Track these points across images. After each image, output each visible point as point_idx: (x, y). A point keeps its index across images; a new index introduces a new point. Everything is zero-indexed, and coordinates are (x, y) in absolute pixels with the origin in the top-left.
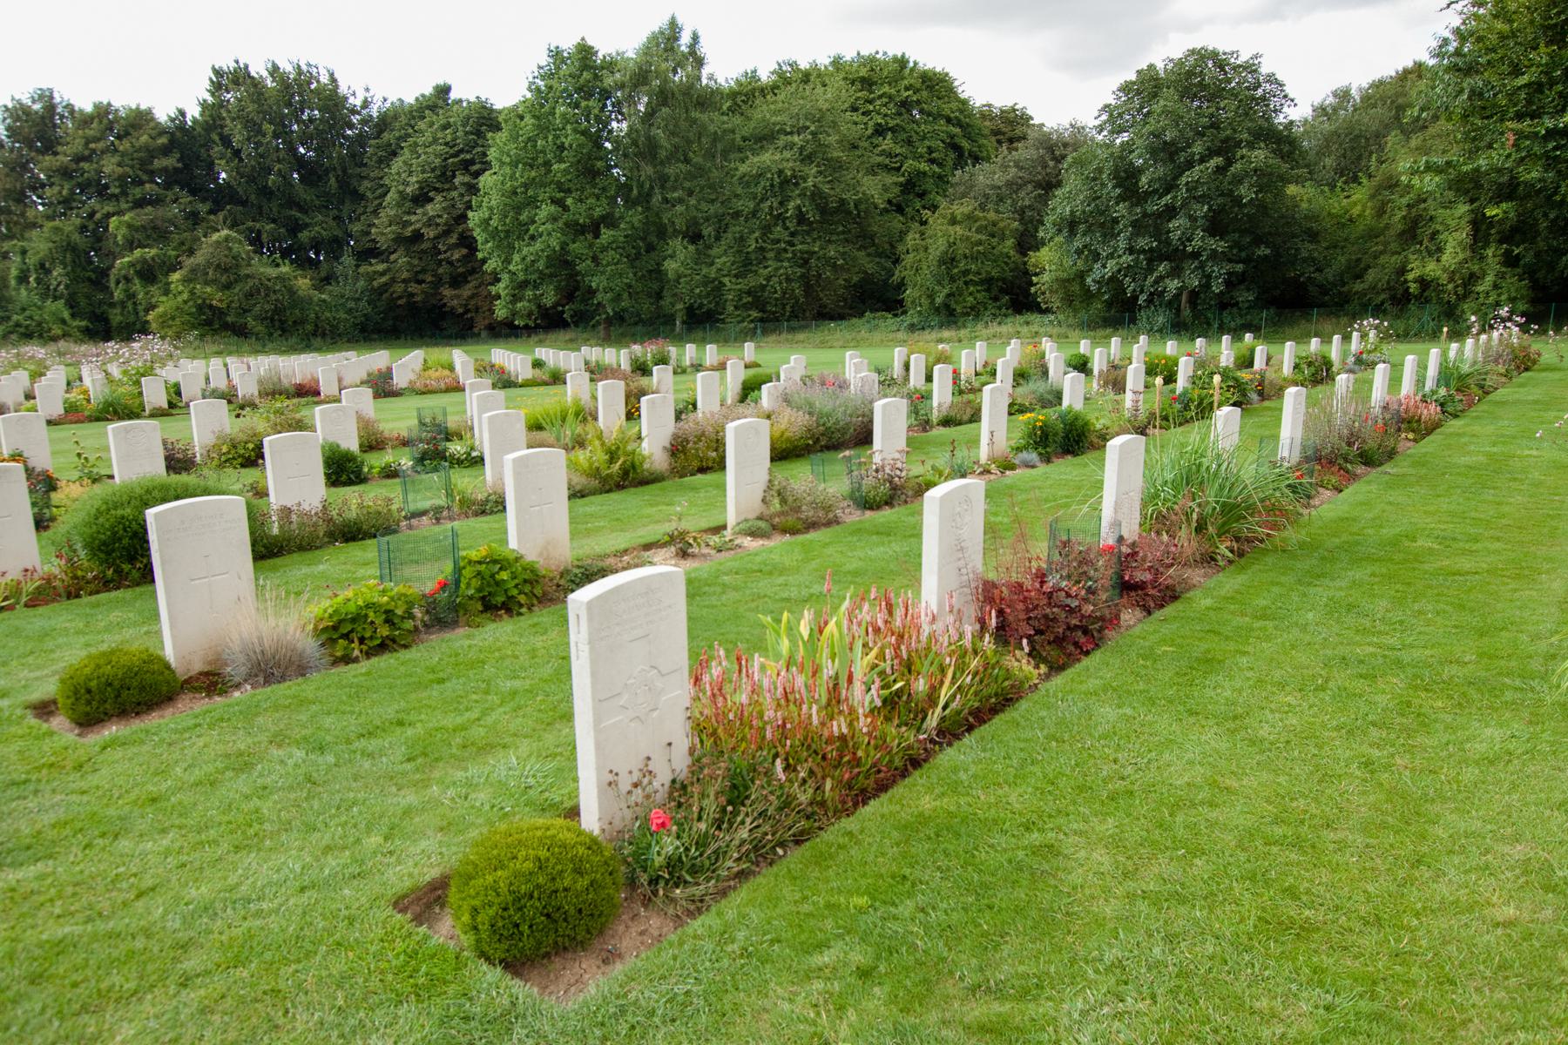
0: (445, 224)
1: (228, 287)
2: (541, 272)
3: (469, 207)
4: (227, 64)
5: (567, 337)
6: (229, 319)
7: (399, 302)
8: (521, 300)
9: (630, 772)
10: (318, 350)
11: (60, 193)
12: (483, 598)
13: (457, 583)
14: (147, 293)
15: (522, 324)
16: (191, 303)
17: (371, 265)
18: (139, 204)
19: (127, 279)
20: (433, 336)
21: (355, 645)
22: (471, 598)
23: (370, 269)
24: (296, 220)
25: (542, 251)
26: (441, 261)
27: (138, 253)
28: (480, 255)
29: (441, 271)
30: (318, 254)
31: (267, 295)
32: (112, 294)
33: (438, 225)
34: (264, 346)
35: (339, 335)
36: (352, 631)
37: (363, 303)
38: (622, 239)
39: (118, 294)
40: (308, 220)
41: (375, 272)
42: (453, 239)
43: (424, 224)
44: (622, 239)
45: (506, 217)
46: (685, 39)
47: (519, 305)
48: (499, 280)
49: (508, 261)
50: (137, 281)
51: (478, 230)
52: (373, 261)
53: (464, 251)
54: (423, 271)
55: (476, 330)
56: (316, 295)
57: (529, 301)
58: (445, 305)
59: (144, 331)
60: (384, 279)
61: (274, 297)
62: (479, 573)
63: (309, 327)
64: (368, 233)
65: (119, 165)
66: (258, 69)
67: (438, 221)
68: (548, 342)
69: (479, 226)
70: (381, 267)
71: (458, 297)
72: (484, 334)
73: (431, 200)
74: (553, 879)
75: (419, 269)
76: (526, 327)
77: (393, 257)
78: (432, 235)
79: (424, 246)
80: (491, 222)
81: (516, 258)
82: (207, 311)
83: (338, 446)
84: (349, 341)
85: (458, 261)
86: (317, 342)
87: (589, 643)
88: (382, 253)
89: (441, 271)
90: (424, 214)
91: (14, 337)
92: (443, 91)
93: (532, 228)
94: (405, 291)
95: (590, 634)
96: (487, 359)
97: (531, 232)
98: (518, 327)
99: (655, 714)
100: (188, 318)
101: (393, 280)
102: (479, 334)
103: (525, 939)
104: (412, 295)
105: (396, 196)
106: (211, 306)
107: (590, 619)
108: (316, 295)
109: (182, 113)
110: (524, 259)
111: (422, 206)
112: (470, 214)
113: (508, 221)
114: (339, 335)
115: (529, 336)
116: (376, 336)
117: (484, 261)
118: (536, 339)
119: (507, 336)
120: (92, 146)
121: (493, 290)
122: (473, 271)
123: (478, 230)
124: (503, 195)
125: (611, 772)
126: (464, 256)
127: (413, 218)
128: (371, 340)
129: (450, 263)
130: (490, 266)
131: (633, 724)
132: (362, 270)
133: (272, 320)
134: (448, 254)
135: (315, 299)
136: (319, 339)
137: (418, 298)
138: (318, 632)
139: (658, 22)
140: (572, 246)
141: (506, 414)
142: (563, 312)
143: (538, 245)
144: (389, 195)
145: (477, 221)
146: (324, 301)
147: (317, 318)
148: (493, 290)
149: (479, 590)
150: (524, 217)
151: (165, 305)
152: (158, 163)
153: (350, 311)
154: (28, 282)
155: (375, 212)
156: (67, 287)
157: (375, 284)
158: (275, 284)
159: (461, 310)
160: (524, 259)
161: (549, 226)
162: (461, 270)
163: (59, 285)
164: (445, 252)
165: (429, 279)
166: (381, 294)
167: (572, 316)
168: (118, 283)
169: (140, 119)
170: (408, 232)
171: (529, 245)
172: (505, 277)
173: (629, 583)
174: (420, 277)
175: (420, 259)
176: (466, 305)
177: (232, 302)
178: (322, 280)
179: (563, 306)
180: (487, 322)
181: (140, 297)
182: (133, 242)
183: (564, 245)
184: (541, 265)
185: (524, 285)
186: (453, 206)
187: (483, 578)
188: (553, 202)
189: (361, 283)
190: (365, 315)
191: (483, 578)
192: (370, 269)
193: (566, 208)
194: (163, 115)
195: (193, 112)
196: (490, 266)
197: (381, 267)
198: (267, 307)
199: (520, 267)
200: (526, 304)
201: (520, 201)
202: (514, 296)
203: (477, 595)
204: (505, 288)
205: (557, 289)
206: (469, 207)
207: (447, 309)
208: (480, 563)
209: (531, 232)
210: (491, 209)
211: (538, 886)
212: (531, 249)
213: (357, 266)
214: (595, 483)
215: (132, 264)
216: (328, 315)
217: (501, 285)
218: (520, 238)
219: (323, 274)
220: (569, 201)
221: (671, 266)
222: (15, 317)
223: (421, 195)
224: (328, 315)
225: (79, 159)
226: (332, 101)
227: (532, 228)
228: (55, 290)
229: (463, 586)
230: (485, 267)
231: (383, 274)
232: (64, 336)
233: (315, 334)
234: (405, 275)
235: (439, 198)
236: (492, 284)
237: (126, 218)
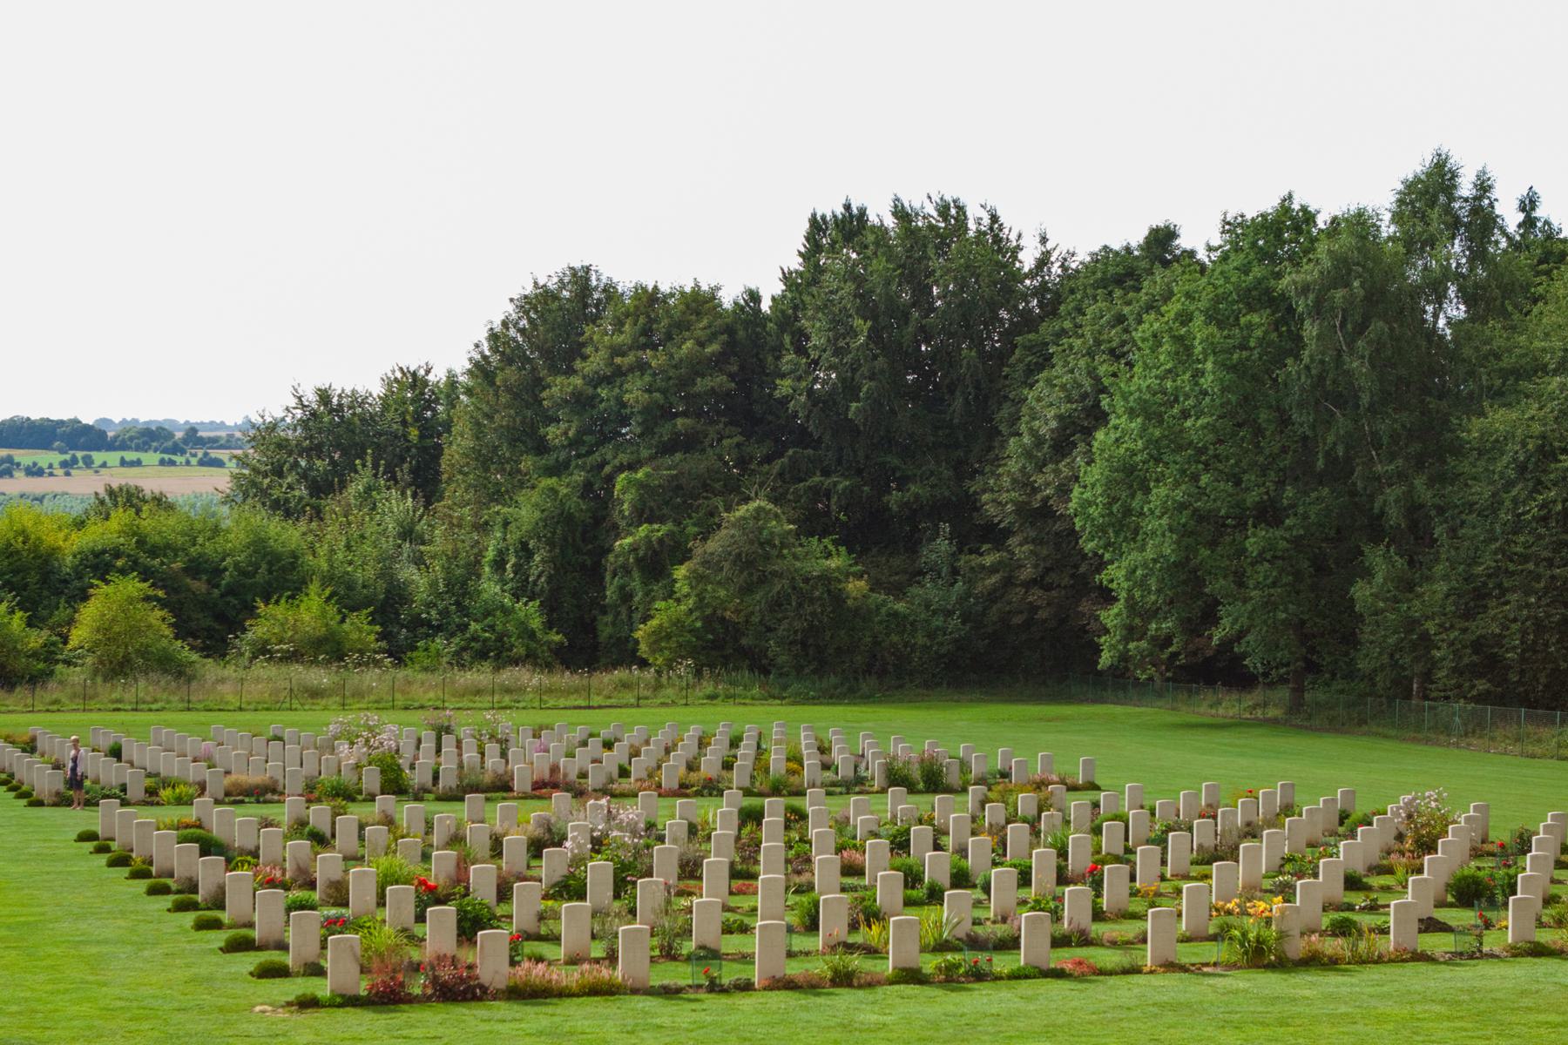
1: (747, 590)
4: (831, 207)
6: (744, 641)
11: (566, 433)
14: (647, 594)
16: (696, 614)
18: (667, 449)
19: (627, 571)
23: (975, 560)
27: (643, 530)
31: (800, 605)
32: (604, 589)
34: (785, 688)
37: (955, 621)
38: (1283, 544)
39: (611, 593)
44: (1283, 544)
46: (1466, 188)
50: (636, 574)
59: (627, 655)
61: (809, 609)
65: (649, 391)
66: (880, 213)
82: (717, 626)
84: (927, 685)
91: (466, 656)
92: (1162, 238)
100: (688, 637)
101: (1008, 582)
104: (1034, 609)
106: (723, 620)
109: (754, 297)
113: (1115, 509)
120: (618, 360)
133: (804, 644)
139: (1415, 164)
151: (664, 613)
152: (702, 384)
153: (931, 635)
154: (505, 570)
156: (550, 579)
158: (814, 588)
163: (539, 576)
165: (1066, 581)
168: (615, 575)
169: (700, 303)
177: (752, 613)
181: (636, 599)
182: (643, 511)
194: (729, 297)
195: (771, 289)
198: (797, 625)
201: (1131, 478)
215: (634, 549)
216: (895, 638)
221: (1361, 592)
222: (474, 626)
224: (895, 638)
225: (598, 380)
226: (995, 243)
228: (535, 583)
231: (993, 570)
232: (527, 656)
233: (868, 671)
237: (640, 475)
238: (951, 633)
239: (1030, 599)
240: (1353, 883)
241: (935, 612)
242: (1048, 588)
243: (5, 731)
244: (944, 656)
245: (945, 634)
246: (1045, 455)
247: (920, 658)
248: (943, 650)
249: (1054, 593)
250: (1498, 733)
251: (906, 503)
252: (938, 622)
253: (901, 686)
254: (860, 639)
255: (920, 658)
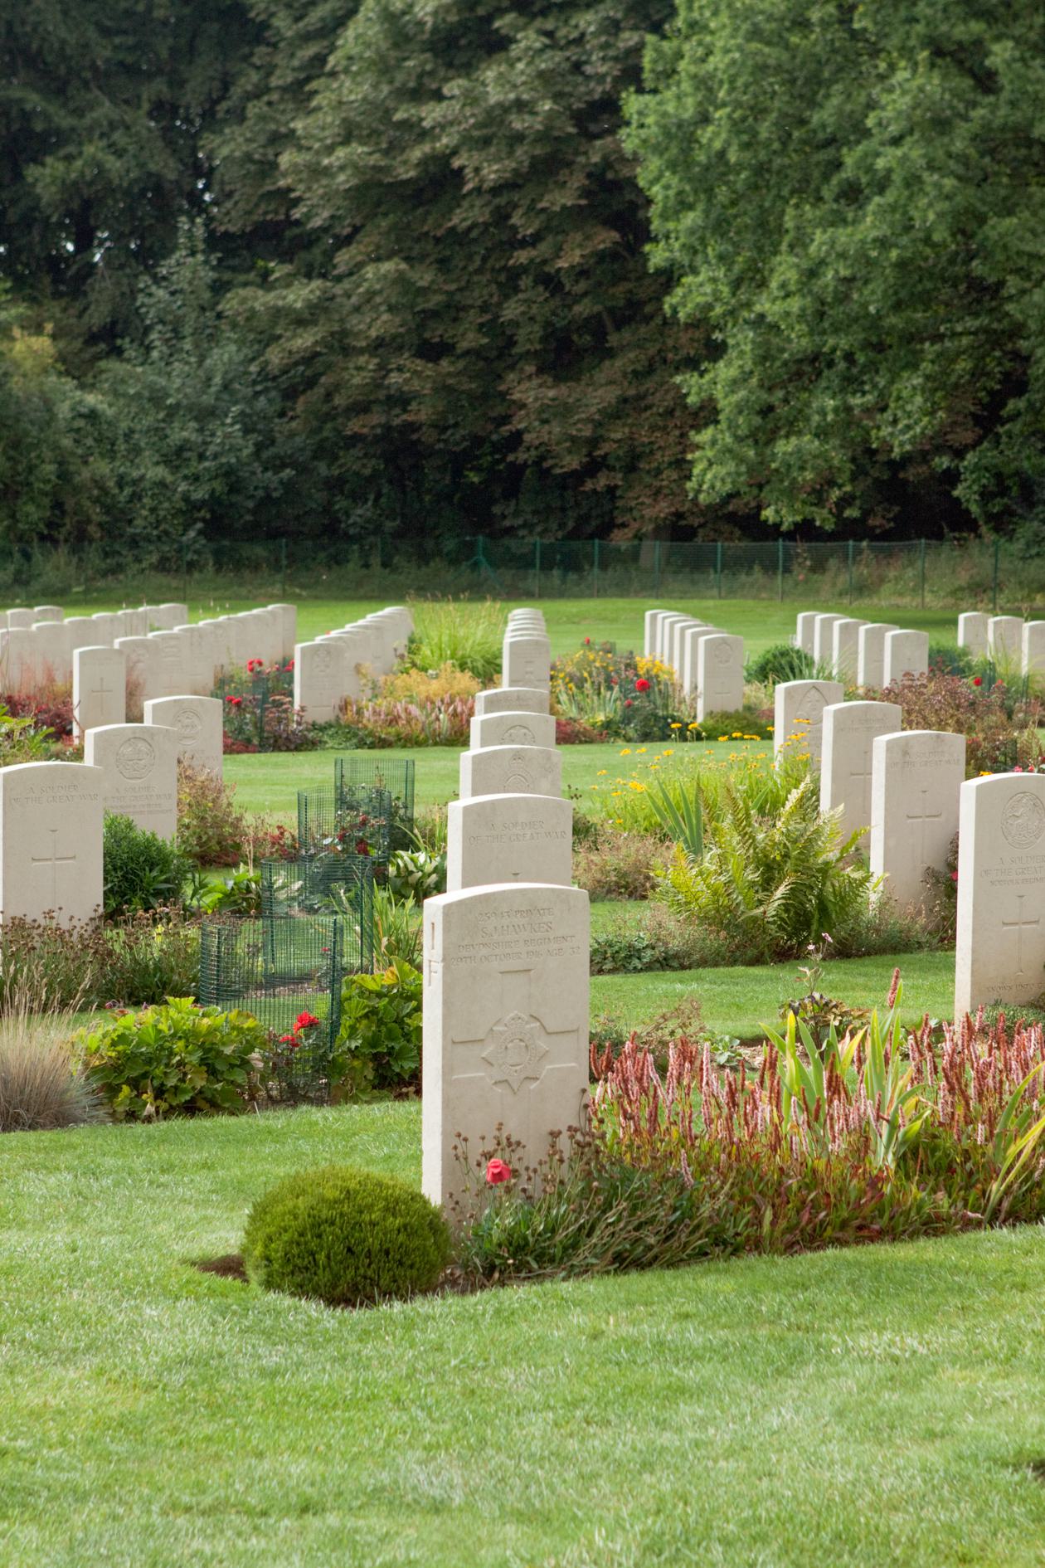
0: (543, 137)
2: (875, 322)
3: (632, 76)
5: (963, 579)
7: (355, 426)
8: (792, 427)
9: (483, 1138)
10: (59, 595)
12: (376, 1057)
13: (335, 1027)
15: (789, 520)
17: (265, 282)
20: (464, 555)
21: (148, 1097)
22: (354, 1053)
23: (262, 300)
24: (26, 116)
25: (883, 243)
26: (515, 274)
28: (657, 256)
29: (511, 310)
30: (85, 243)
33: (519, 138)
35: (134, 542)
36: (145, 1075)
37: (227, 432)
40: (65, 121)
41: (277, 313)
42: (563, 197)
43: (467, 141)
45: (759, 111)
47: (784, 447)
48: (716, 351)
49: (753, 278)
51: (654, 163)
52: (279, 270)
53: (606, 238)
54: (452, 310)
55: (620, 540)
56: (71, 398)
57: (822, 433)
58: (516, 438)
60: (304, 340)
62: (374, 1011)
63: (33, 513)
64: (269, 168)
67: (518, 123)
68: (885, 598)
69: (659, 150)
70: (299, 295)
71: (564, 411)
72: (654, 552)
73: (498, 45)
74: (361, 1212)
75: (436, 300)
76: (805, 530)
77: (343, 258)
78: (492, 173)
79: (459, 218)
80: (705, 134)
81: (785, 269)
83: (130, 826)
84: (163, 566)
85: (582, 273)
86: (54, 565)
87: (444, 960)
88: (309, 241)
89: (511, 310)
90: (471, 99)
93: (850, 158)
94: (377, 385)
95: (445, 948)
96: (623, 645)
97: (847, 173)
98: (773, 532)
99: (534, 1085)
101: (341, 344)
102: (635, 555)
103: (320, 1272)
105: (374, 32)
107: (447, 930)
108: (71, 398)
110: (812, 273)
111: (467, 69)
112: (632, 103)
114: (134, 542)
115: (819, 567)
116: (259, 551)
117: (669, 278)
118: (843, 580)
119: (737, 565)
121: (692, 386)
122: (633, 312)
123: (654, 163)
124: (755, 34)
125: (459, 1135)
126: (601, 257)
127: (431, 114)
128: (239, 565)
129: (551, 282)
130: (686, 300)
131: (498, 1090)
132: (231, 303)
134: (544, 248)
135: (64, 410)
136: (61, 555)
137: (421, 413)
138: (92, 1072)
140: (1000, 227)
141: (518, 756)
142: (952, 477)
143: (870, 224)
144: (350, 32)
145: (653, 131)
146: (92, 416)
147: (64, 476)
148: (692, 386)
149: (373, 1042)
150: (825, 116)
153: (175, 457)
155: (299, 93)
157: (274, 357)
159: (572, 462)
160: (812, 273)
161: (914, 151)
162: (583, 309)
164: (536, 239)
166: (291, 394)
167: (985, 496)
170: (407, 166)
171: (838, 220)
172: (742, 341)
173: (494, 894)
174: (435, 332)
175: (443, 264)
176: (594, 442)
178: (92, 339)
179: (959, 454)
180: (663, 508)
183: (966, 224)
184: (872, 298)
185: (809, 369)
186: (577, 67)
187: (381, 1022)
188: (939, 51)
189: (225, 355)
190: (228, 473)
191: (381, 1022)
192: (262, 300)
193: (986, 82)
196: (686, 300)
197: (299, 295)
199: (795, 304)
200: (808, 443)
202: (767, 411)
203: (366, 1051)
204: (734, 384)
205: (935, 384)
206: (632, 76)
207: (521, 456)
208: (380, 995)
209: (847, 173)
210: (704, 84)
211: (342, 1215)
212: (843, 235)
213: (219, 288)
214: (717, 940)
217: (725, 370)
218: (806, 190)
219: (98, 316)
220: (1000, 54)
223: (464, 27)
227: (850, 158)
229: (343, 1032)
230: (669, 302)
234: (381, 324)
235: (528, 39)
236: (692, 364)
238: (216, 456)
239: (394, 378)
240: (660, 1344)
241: (172, 412)
242: (432, 351)
243: (14, 679)
244: (203, 503)
245: (201, 457)
246: (484, 84)
247: (153, 510)
248: (200, 494)
249: (445, 365)
250: (824, 581)
251: (75, 183)
252: (183, 432)
253: (118, 569)
254: (31, 469)
255: (153, 510)
